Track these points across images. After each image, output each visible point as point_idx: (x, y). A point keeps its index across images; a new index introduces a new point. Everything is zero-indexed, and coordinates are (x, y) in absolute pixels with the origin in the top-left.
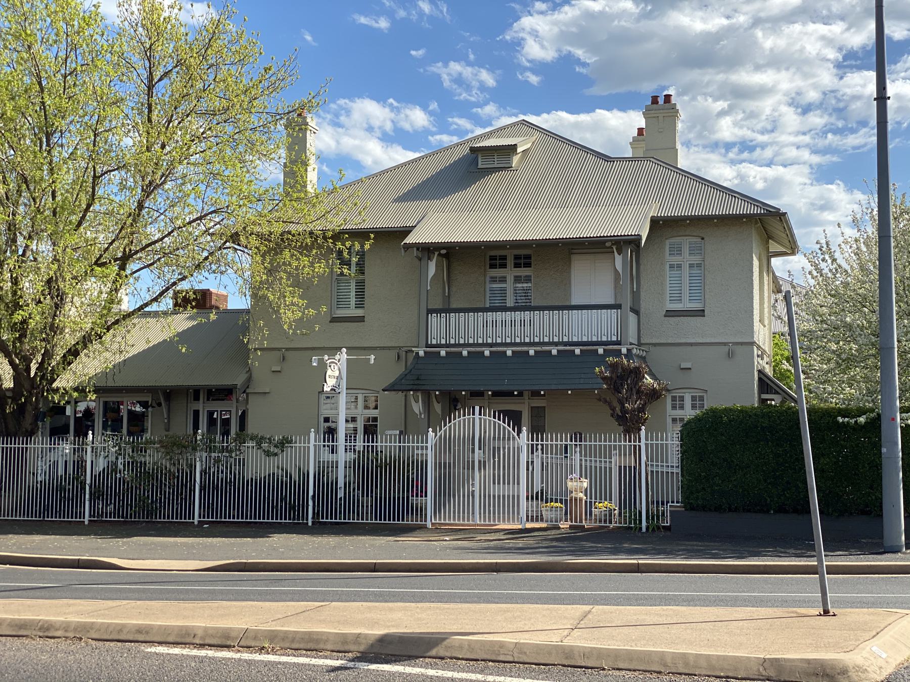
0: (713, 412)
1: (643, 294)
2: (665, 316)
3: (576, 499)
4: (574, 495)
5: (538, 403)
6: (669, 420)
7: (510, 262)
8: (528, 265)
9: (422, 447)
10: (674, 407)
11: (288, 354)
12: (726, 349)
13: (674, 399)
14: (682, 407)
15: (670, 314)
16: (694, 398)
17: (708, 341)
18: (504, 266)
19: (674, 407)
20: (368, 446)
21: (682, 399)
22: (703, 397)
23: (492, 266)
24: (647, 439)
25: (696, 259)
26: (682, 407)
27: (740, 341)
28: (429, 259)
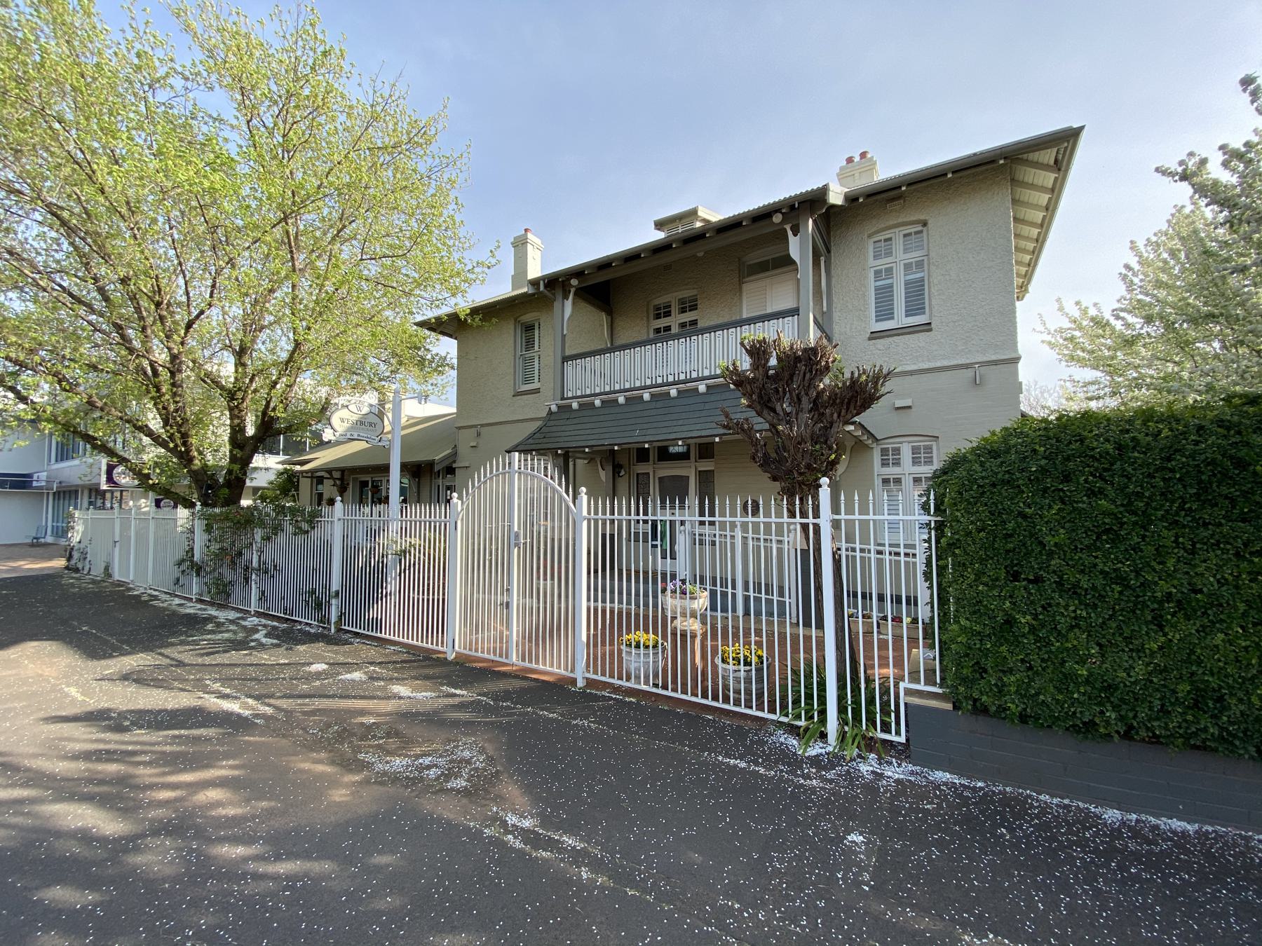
0: (955, 464)
1: (836, 315)
2: (870, 339)
3: (684, 635)
4: (678, 623)
5: (706, 465)
6: (878, 482)
7: (675, 309)
8: (694, 308)
9: (723, 524)
10: (885, 464)
11: (484, 430)
12: (969, 373)
13: (884, 452)
14: (897, 463)
15: (875, 336)
16: (915, 450)
17: (938, 364)
18: (668, 314)
19: (885, 464)
20: (612, 521)
21: (897, 451)
22: (931, 448)
23: (658, 317)
24: (835, 509)
25: (914, 256)
26: (897, 463)
27: (994, 358)
28: (566, 297)
